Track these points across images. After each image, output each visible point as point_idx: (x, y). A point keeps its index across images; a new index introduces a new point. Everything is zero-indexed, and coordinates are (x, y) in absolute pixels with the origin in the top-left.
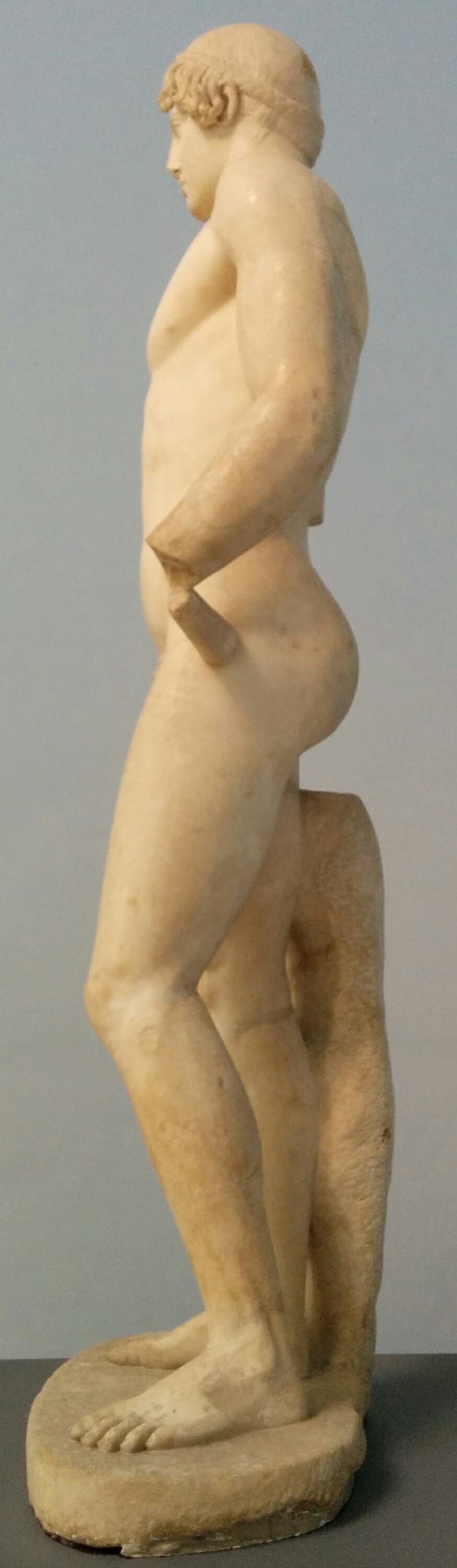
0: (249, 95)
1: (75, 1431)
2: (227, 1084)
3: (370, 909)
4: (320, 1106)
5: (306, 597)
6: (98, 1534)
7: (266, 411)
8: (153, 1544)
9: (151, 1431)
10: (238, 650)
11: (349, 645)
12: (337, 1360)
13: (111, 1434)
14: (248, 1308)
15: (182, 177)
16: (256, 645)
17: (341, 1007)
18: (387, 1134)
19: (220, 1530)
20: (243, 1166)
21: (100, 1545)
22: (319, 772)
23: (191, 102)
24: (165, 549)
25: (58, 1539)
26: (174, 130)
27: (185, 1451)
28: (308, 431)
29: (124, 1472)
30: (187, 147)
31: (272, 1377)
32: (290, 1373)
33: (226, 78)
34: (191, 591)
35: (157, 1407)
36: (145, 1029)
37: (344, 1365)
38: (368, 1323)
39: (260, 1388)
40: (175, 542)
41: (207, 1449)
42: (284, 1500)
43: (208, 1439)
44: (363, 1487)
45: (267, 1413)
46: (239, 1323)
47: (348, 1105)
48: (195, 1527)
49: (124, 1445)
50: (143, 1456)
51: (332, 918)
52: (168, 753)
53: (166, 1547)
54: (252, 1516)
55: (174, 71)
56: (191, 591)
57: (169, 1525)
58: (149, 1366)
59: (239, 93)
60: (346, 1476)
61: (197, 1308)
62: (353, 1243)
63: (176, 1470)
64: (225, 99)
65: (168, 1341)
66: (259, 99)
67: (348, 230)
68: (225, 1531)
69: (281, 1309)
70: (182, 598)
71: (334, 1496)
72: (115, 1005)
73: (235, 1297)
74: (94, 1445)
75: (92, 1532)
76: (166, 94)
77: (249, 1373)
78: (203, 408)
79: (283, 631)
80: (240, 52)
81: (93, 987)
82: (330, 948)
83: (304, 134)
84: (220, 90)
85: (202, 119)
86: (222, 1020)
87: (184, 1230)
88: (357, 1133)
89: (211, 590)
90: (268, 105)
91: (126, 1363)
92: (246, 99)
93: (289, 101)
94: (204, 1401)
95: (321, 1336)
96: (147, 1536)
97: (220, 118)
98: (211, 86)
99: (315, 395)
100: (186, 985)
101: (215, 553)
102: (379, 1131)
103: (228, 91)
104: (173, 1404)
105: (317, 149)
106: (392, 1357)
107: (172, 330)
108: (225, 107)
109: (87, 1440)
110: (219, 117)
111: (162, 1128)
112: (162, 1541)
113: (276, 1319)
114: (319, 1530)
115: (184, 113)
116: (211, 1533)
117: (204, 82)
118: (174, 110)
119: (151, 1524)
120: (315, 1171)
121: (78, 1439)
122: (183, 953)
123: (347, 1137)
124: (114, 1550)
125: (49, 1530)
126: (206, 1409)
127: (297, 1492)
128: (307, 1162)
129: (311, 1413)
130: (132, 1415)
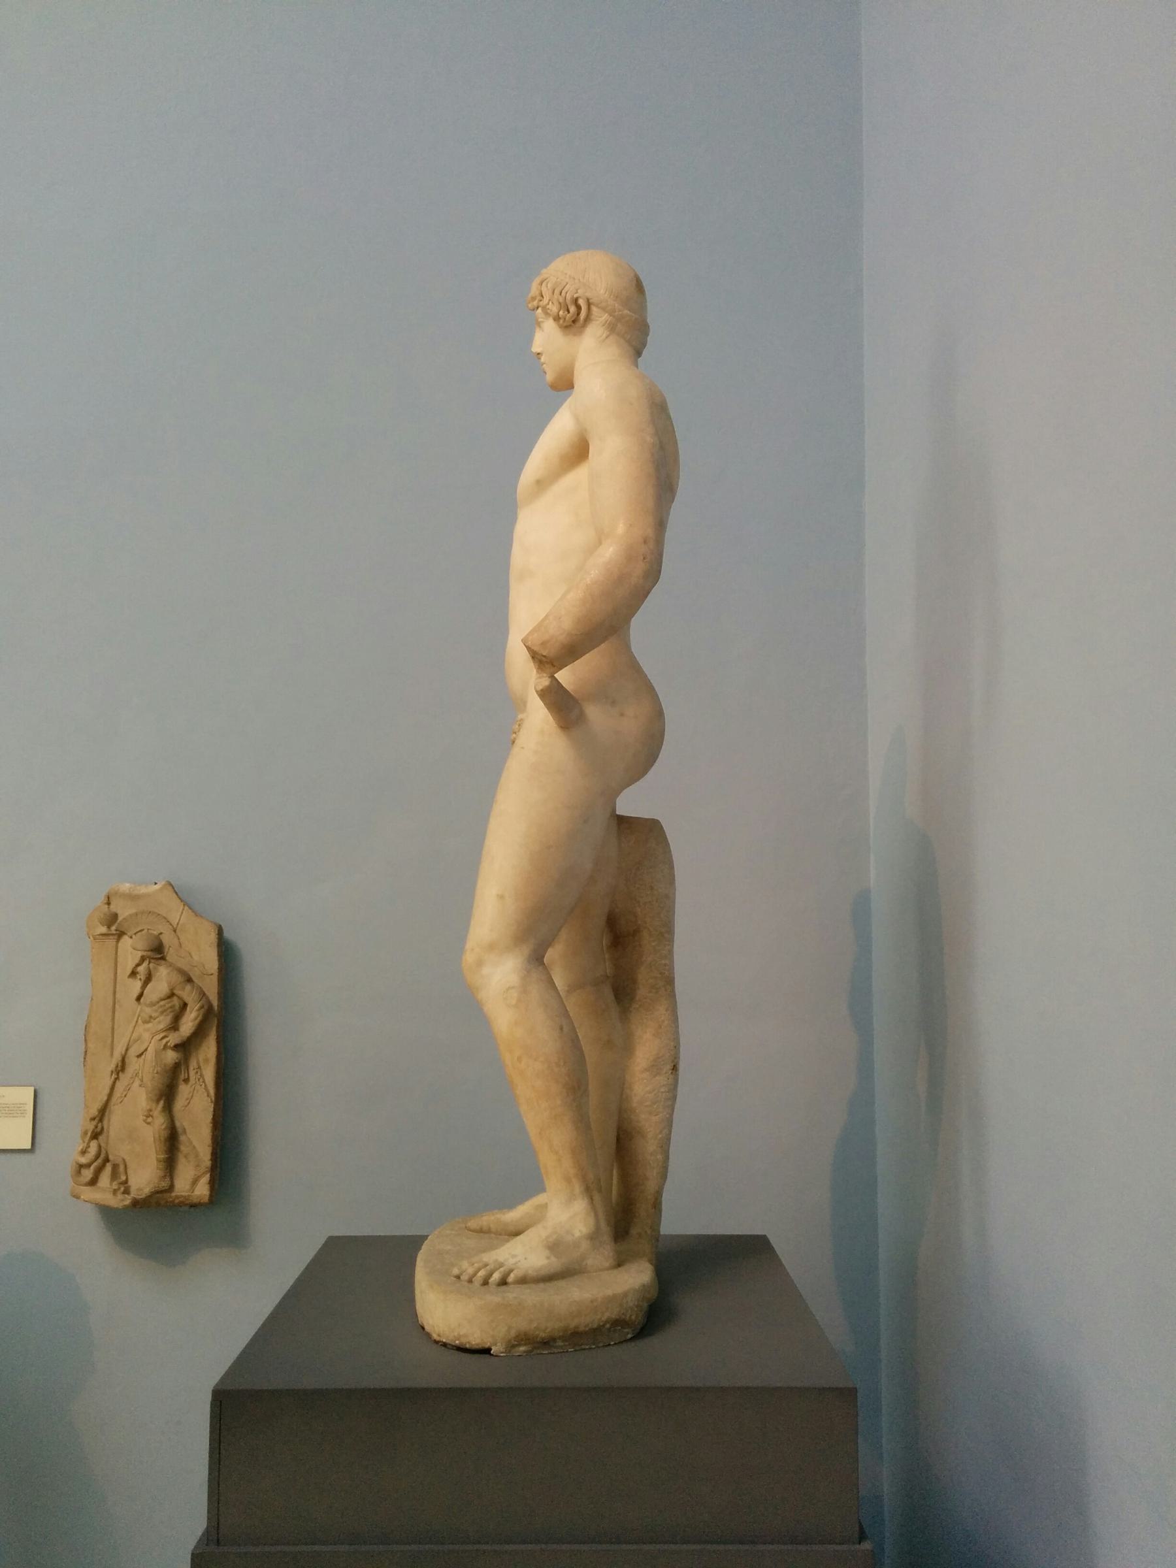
0: (597, 306)
1: (456, 1271)
2: (566, 1029)
3: (666, 904)
4: (628, 1048)
5: (631, 678)
6: (475, 1338)
7: (609, 552)
8: (514, 1346)
9: (511, 1271)
10: (581, 718)
11: (660, 714)
12: (634, 1231)
13: (482, 1273)
14: (578, 1188)
16: (594, 713)
17: (644, 976)
18: (675, 1068)
19: (560, 1338)
20: (576, 1088)
22: (630, 804)
23: (554, 308)
24: (536, 648)
25: (445, 1345)
26: (539, 324)
27: (533, 1286)
28: (639, 568)
29: (494, 1297)
30: (547, 338)
31: (593, 1237)
32: (606, 1237)
34: (552, 677)
35: (514, 1256)
36: (509, 988)
37: (640, 1235)
38: (657, 1205)
39: (585, 1245)
40: (543, 644)
41: (548, 1284)
42: (604, 1319)
43: (548, 1278)
44: (654, 1316)
45: (590, 1262)
46: (571, 1198)
47: (647, 1047)
48: (543, 1335)
49: (491, 1280)
50: (504, 1288)
51: (639, 910)
52: (528, 789)
53: (522, 1349)
54: (582, 1329)
55: (541, 284)
56: (552, 677)
57: (526, 1334)
58: (498, 1233)
59: (589, 304)
60: (645, 1305)
61: (538, 1187)
62: (648, 1147)
63: (531, 1297)
64: (579, 308)
65: (513, 1216)
66: (604, 309)
67: (669, 418)
68: (563, 1338)
69: (600, 1191)
70: (545, 682)
71: (637, 1317)
72: (486, 970)
73: (568, 1180)
74: (470, 1281)
75: (471, 1339)
76: (533, 299)
77: (577, 1234)
78: (559, 542)
79: (614, 703)
80: (589, 272)
81: (469, 958)
82: (636, 932)
83: (634, 335)
84: (576, 301)
86: (560, 981)
87: (532, 1131)
88: (654, 1068)
89: (565, 676)
92: (594, 309)
93: (626, 312)
94: (547, 1253)
95: (625, 1212)
96: (510, 1341)
97: (574, 322)
98: (569, 297)
99: (645, 542)
100: (537, 959)
101: (571, 651)
102: (669, 1067)
103: (581, 302)
104: (525, 1254)
105: (644, 345)
106: (673, 1237)
107: (539, 482)
108: (578, 314)
109: (465, 1277)
110: (574, 319)
111: (519, 1059)
112: (519, 1345)
113: (597, 1197)
114: (626, 1341)
115: (546, 313)
116: (554, 1340)
118: (540, 310)
119: (513, 1333)
120: (622, 1095)
121: (458, 1277)
122: (534, 935)
123: (646, 1070)
124: (486, 1351)
125: (438, 1339)
126: (548, 1258)
127: (612, 1313)
128: (617, 1086)
129: (619, 1264)
130: (496, 1261)
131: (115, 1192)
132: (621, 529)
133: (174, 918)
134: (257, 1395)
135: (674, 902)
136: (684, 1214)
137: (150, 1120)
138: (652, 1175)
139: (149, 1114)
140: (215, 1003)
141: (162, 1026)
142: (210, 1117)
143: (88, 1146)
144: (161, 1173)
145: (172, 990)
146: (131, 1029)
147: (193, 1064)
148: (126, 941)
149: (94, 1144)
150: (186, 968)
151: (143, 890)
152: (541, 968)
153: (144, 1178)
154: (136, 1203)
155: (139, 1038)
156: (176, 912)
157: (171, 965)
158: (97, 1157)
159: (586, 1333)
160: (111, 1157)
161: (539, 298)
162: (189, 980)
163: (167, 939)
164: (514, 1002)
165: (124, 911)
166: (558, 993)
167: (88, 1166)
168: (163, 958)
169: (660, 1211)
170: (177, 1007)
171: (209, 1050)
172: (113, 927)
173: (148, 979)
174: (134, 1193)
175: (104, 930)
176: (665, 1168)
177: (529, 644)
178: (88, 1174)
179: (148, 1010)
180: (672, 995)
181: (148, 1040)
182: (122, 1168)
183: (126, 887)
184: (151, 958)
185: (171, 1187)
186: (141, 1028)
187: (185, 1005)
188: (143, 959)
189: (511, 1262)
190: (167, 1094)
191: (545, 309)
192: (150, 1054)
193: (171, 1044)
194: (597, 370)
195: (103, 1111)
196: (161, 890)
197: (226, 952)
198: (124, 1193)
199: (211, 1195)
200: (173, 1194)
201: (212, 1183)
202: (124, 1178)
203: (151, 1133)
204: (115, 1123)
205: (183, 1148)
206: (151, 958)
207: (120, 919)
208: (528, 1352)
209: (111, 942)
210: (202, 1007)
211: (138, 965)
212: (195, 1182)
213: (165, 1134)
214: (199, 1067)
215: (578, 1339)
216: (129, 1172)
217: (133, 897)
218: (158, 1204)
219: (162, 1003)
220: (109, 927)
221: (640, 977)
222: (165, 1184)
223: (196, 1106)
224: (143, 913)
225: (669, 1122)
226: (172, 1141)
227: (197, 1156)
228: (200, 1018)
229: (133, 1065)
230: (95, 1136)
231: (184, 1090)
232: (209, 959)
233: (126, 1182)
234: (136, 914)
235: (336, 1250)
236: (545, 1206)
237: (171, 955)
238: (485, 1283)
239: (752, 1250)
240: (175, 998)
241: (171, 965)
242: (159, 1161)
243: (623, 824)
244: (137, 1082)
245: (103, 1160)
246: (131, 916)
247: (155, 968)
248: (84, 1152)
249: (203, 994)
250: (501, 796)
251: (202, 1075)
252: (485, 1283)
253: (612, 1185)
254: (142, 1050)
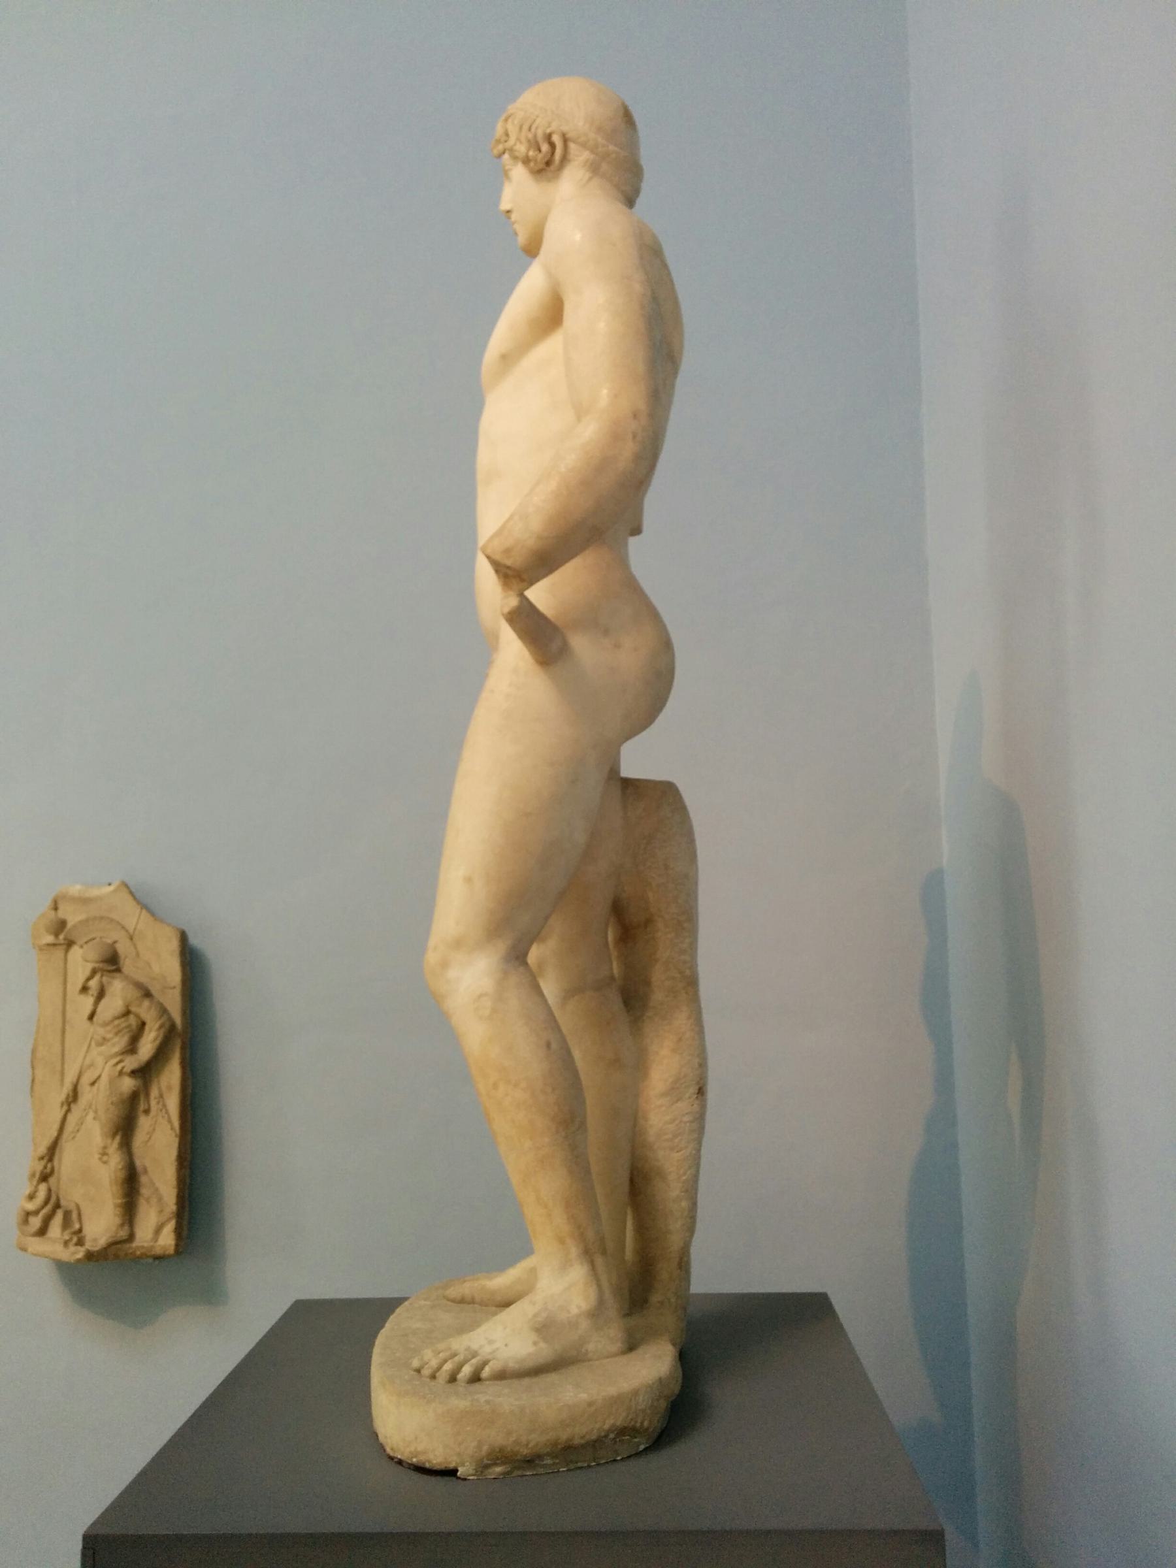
1: (416, 1363)
2: (554, 1046)
4: (640, 1066)
5: (628, 601)
6: (437, 1457)
7: (590, 431)
8: (487, 1467)
9: (485, 1363)
10: (564, 650)
11: (666, 645)
12: (655, 1298)
13: (448, 1367)
14: (574, 1251)
15: (514, 217)
16: (581, 644)
17: (658, 976)
18: (701, 1092)
19: (548, 1454)
20: (569, 1120)
21: (438, 1467)
22: (639, 760)
23: (521, 149)
24: (497, 557)
25: (400, 1462)
26: (506, 174)
28: (629, 449)
30: (518, 190)
31: (596, 1314)
33: (554, 127)
34: (521, 595)
35: (491, 1342)
36: (481, 996)
37: (662, 1303)
38: (684, 1264)
39: (584, 1324)
40: (507, 551)
41: (535, 1380)
42: (606, 1427)
44: (679, 1414)
45: (591, 1347)
46: (565, 1266)
47: (665, 1065)
48: (525, 1451)
49: (460, 1376)
50: (477, 1386)
51: (650, 895)
52: (502, 740)
53: (499, 1469)
54: (577, 1441)
55: (506, 120)
56: (521, 595)
57: (501, 1450)
58: (483, 1304)
59: (565, 140)
60: (663, 1404)
62: (670, 1192)
63: (507, 1399)
64: (552, 146)
66: (584, 145)
69: (604, 1252)
70: (513, 602)
71: (652, 1423)
72: (452, 973)
73: (562, 1241)
74: (433, 1377)
75: (431, 1457)
76: (498, 142)
77: (574, 1311)
78: (532, 430)
79: (606, 632)
80: (564, 102)
81: (432, 958)
82: (649, 922)
83: (626, 179)
84: (549, 138)
86: (550, 988)
87: (515, 1180)
88: (673, 1092)
89: (540, 594)
90: (592, 152)
91: (462, 1301)
93: (611, 148)
94: (533, 1336)
96: (482, 1460)
97: (548, 163)
98: (540, 133)
99: (635, 416)
100: (517, 956)
101: (544, 561)
102: (693, 1090)
103: (556, 139)
104: (505, 1339)
105: (637, 191)
108: (553, 153)
109: (426, 1372)
110: (547, 162)
111: (495, 1086)
112: (495, 1464)
113: (599, 1260)
114: (638, 1454)
116: (540, 1457)
117: (533, 130)
118: (506, 156)
120: (635, 1126)
121: (418, 1371)
122: (514, 927)
123: (664, 1095)
124: (451, 1473)
125: (392, 1454)
127: (619, 1419)
129: (631, 1346)
130: (468, 1349)
131: (66, 1243)
132: (604, 394)
133: (131, 923)
134: (136, 1542)
135: (696, 884)
136: (723, 1262)
137: (105, 1158)
138: (675, 1227)
139: (104, 1153)
140: (178, 1020)
141: (116, 1049)
142: (174, 1153)
143: (35, 1192)
144: (118, 1221)
145: (127, 1006)
146: (82, 1054)
147: (154, 1093)
148: (76, 953)
149: (43, 1188)
150: (142, 979)
151: (95, 892)
152: (522, 969)
153: (101, 1226)
154: (90, 1256)
155: (92, 1065)
156: (132, 917)
157: (127, 978)
158: (46, 1202)
159: (583, 1446)
160: (63, 1203)
161: (504, 138)
162: (148, 994)
163: (123, 948)
165: (73, 916)
166: (546, 1001)
167: (36, 1213)
168: (118, 970)
169: (688, 1272)
170: (134, 1027)
171: (171, 1076)
172: (62, 935)
173: (101, 995)
174: (88, 1245)
175: (50, 939)
176: (692, 1218)
177: (489, 551)
178: (36, 1222)
179: (101, 1031)
180: (695, 999)
181: (101, 1066)
182: (74, 1216)
183: (76, 889)
184: (103, 970)
185: (131, 1237)
186: (95, 1051)
187: (144, 1024)
188: (94, 972)
189: (497, 1348)
190: (125, 1129)
191: (511, 150)
192: (105, 1079)
193: (128, 1069)
194: (573, 219)
195: (53, 1150)
196: (115, 891)
197: (192, 963)
198: (76, 1244)
199: (177, 1245)
200: (134, 1245)
201: (178, 1231)
202: (77, 1226)
203: (109, 1172)
204: (67, 1162)
205: (145, 1191)
206: (103, 970)
207: (69, 925)
208: (506, 1474)
209: (59, 953)
210: (161, 1027)
211: (89, 979)
212: (158, 1230)
213: (121, 1175)
214: (161, 1096)
215: (573, 1455)
216: (84, 1218)
217: (84, 901)
218: (116, 1256)
219: (117, 1022)
220: (57, 935)
221: (653, 979)
222: (123, 1234)
223: (159, 1141)
224: (95, 918)
225: (696, 1160)
226: (131, 1183)
227: (160, 1199)
228: (158, 1042)
229: (87, 1095)
230: (44, 1178)
231: (144, 1123)
232: (169, 969)
233: (80, 1231)
234: (87, 920)
235: (303, 1313)
236: (533, 1271)
237: (127, 966)
238: (453, 1379)
239: (808, 1312)
240: (132, 1017)
241: (127, 978)
242: (116, 1206)
243: (630, 787)
244: (91, 1115)
245: (53, 1204)
246: (80, 922)
247: (109, 983)
248: (31, 1197)
249: (164, 1011)
250: (467, 754)
251: (164, 1106)
252: (453, 1379)
253: (624, 1241)
254: (95, 1077)
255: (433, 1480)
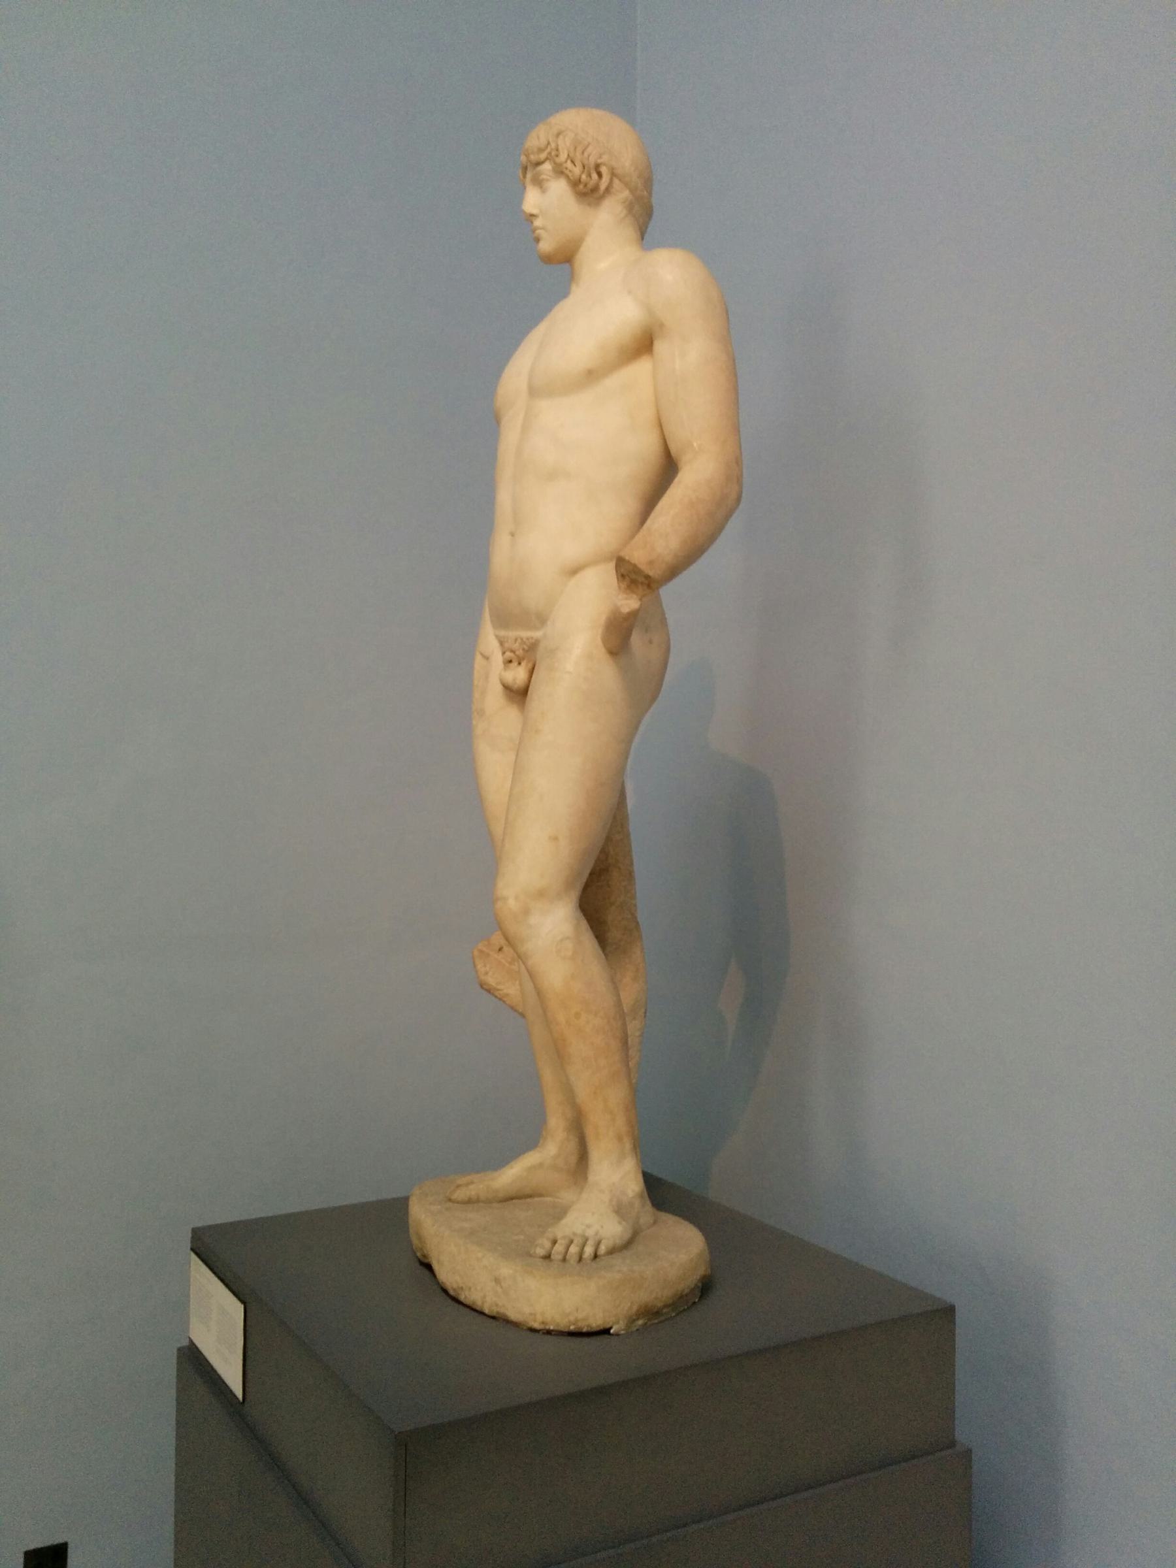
8: (634, 1321)
9: (598, 1244)
13: (574, 1249)
14: (628, 1145)
15: (538, 223)
21: (595, 1329)
33: (605, 158)
35: (589, 1226)
36: (562, 940)
40: (651, 563)
59: (613, 174)
63: (622, 1266)
64: (600, 175)
66: (626, 185)
72: (534, 920)
73: (620, 1139)
77: (631, 1194)
85: (581, 187)
90: (631, 191)
91: (469, 1202)
98: (592, 161)
103: (604, 170)
111: (578, 1016)
117: (586, 154)
118: (547, 166)
119: (635, 1308)
121: (548, 1257)
124: (606, 1332)
164: (570, 953)
255: (586, 1340)
